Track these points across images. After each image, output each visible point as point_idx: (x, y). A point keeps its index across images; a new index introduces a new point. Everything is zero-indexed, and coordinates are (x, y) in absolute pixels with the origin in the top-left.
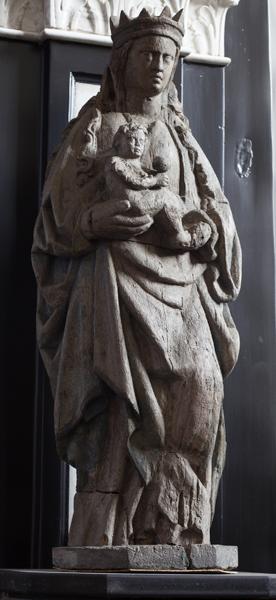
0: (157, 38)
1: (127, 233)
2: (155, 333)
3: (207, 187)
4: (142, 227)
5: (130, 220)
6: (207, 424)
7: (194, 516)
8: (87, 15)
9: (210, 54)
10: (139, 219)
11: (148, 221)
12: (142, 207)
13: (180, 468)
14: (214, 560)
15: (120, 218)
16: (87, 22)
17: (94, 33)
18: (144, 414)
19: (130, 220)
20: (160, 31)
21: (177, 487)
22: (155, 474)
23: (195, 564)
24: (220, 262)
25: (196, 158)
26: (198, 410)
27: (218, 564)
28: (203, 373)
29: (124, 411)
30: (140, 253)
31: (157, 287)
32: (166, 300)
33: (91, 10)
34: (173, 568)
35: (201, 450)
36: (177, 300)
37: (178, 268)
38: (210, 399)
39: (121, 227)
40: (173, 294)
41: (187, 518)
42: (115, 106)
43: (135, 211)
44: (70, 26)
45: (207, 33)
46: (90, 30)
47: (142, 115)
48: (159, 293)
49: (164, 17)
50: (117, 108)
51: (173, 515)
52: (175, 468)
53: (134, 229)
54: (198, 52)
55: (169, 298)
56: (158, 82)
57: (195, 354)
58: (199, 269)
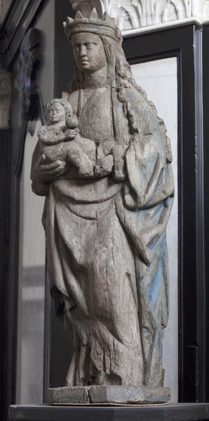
2: (70, 243)
4: (56, 170)
5: (47, 166)
6: (106, 300)
7: (113, 364)
8: (127, 18)
9: (186, 17)
11: (61, 164)
12: (52, 157)
13: (100, 331)
14: (105, 395)
16: (128, 23)
17: (133, 29)
18: (72, 296)
19: (47, 166)
20: (77, 29)
21: (100, 344)
22: (88, 336)
23: (93, 400)
24: (126, 180)
26: (97, 291)
27: (108, 399)
28: (98, 263)
29: (64, 298)
31: (78, 208)
32: (83, 215)
34: (79, 402)
35: (109, 318)
36: (93, 215)
38: (102, 281)
39: (46, 172)
40: (92, 210)
41: (108, 365)
44: (140, 25)
45: (136, 8)
46: (131, 27)
48: (78, 211)
51: (99, 365)
52: (97, 332)
54: (186, 17)
55: (85, 214)
56: (85, 64)
57: (96, 250)
58: (115, 189)
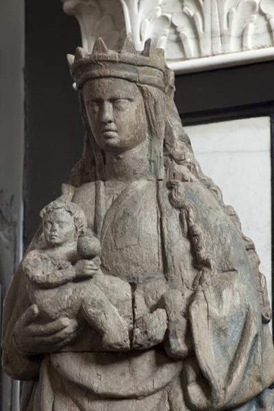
0: (96, 82)
1: (56, 346)
3: (199, 255)
5: (42, 328)
8: (174, 37)
10: (51, 326)
11: (68, 324)
12: (51, 310)
15: (33, 328)
17: (185, 59)
19: (42, 328)
20: (96, 72)
24: (191, 356)
25: (181, 216)
30: (74, 367)
33: (178, 30)
37: (128, 376)
39: (37, 339)
42: (95, 173)
43: (44, 317)
46: (181, 56)
47: (117, 179)
49: (96, 54)
50: (98, 178)
53: (50, 338)
58: (168, 373)
